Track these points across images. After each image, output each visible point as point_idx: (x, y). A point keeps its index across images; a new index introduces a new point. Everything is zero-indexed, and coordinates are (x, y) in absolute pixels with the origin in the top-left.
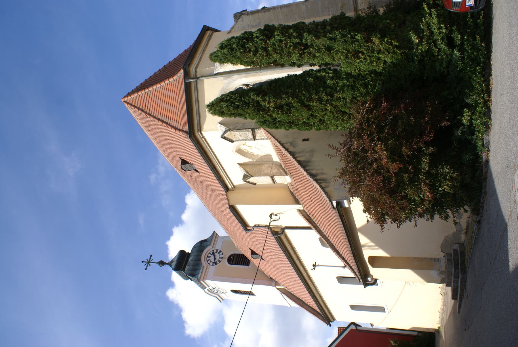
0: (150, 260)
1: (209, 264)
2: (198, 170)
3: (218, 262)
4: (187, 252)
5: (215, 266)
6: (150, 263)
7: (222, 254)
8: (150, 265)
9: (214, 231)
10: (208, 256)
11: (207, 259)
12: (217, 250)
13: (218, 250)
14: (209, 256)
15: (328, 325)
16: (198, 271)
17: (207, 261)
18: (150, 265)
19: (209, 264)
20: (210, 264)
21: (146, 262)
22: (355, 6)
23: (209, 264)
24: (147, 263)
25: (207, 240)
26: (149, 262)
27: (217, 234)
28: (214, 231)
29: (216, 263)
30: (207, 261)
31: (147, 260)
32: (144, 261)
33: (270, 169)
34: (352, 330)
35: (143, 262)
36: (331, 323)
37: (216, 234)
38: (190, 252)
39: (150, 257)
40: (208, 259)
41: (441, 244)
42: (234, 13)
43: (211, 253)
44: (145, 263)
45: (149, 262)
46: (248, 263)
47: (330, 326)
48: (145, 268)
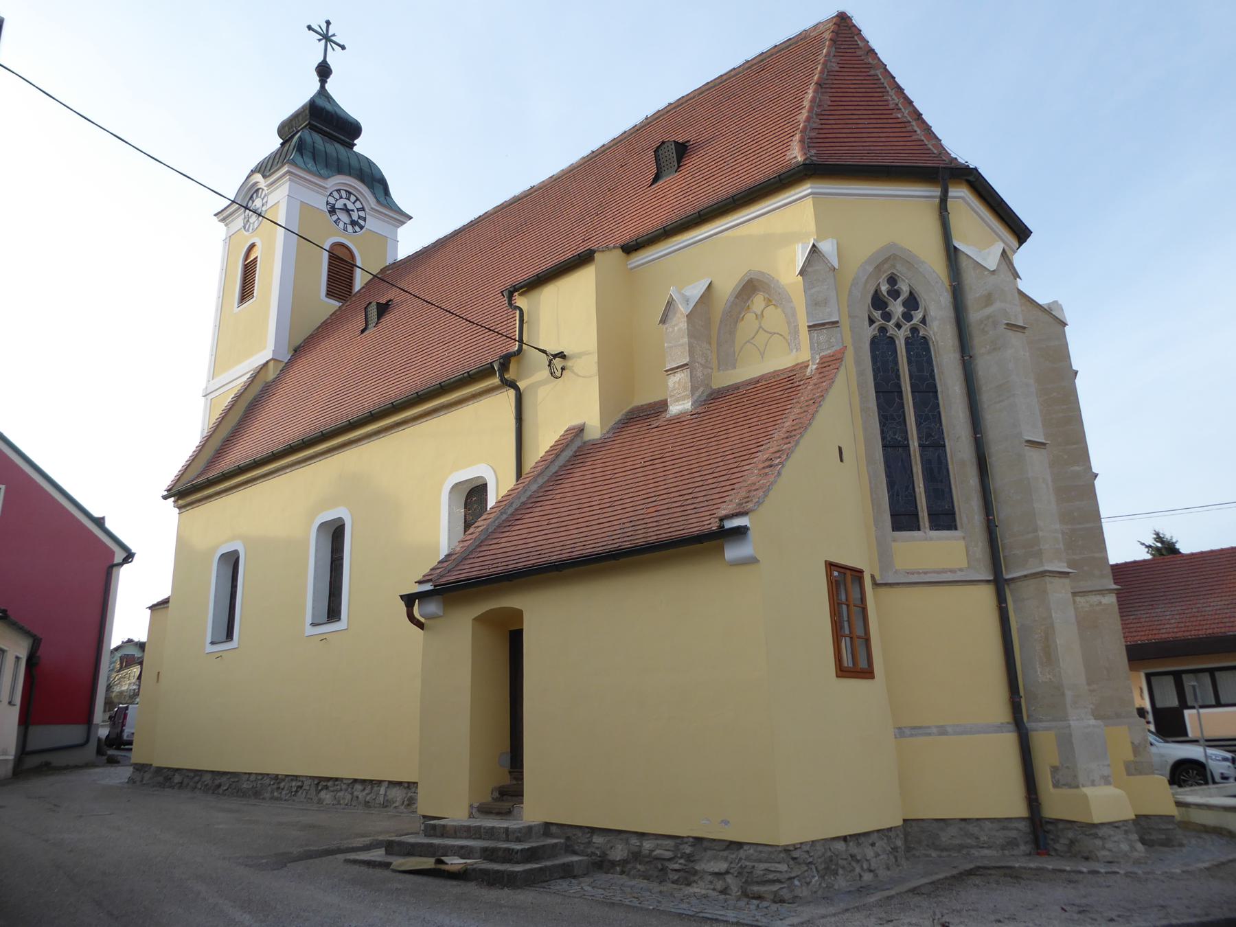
0: (332, 44)
1: (331, 194)
2: (660, 182)
3: (335, 218)
4: (355, 142)
5: (324, 208)
6: (324, 41)
7: (337, 191)
8: (320, 40)
9: (411, 218)
10: (350, 193)
11: (342, 191)
12: (365, 220)
13: (365, 221)
14: (350, 197)
15: (168, 491)
16: (313, 163)
18: (320, 40)
19: (330, 195)
21: (327, 30)
23: (331, 193)
24: (325, 32)
25: (387, 198)
26: (327, 38)
27: (403, 223)
28: (411, 218)
29: (332, 210)
30: (337, 191)
32: (330, 26)
33: (703, 362)
34: (112, 553)
35: (328, 23)
36: (172, 499)
37: (404, 220)
38: (355, 149)
39: (342, 44)
40: (344, 194)
42: (1060, 302)
43: (358, 202)
44: (324, 27)
45: (327, 38)
46: (330, 295)
47: (165, 498)
48: (313, 27)
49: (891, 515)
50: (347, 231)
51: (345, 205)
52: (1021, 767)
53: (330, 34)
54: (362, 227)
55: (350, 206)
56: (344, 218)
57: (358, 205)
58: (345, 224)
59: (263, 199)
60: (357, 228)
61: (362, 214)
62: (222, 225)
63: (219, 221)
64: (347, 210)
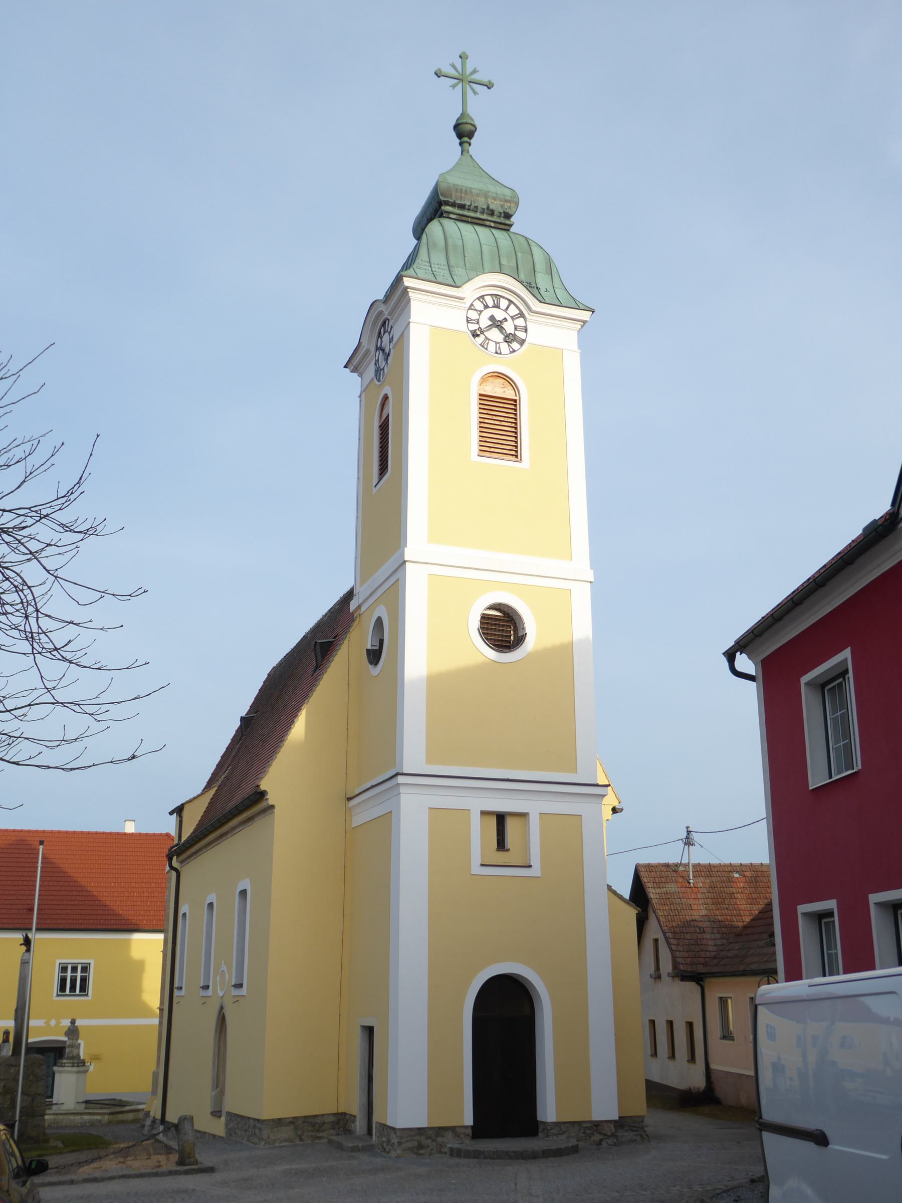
1: (471, 307)
7: (514, 351)
8: (454, 86)
11: (486, 297)
13: (526, 331)
14: (499, 302)
17: (481, 298)
18: (454, 86)
19: (470, 308)
20: (470, 311)
22: (380, 339)
23: (472, 305)
30: (478, 299)
31: (475, 71)
41: (88, 1149)
49: (773, 924)
50: (500, 353)
51: (492, 318)
52: (822, 910)
53: (468, 72)
54: (522, 342)
55: (499, 315)
56: (495, 335)
57: (513, 311)
58: (496, 343)
59: (389, 333)
60: (515, 345)
61: (520, 322)
62: (355, 375)
63: (351, 372)
64: (497, 324)
